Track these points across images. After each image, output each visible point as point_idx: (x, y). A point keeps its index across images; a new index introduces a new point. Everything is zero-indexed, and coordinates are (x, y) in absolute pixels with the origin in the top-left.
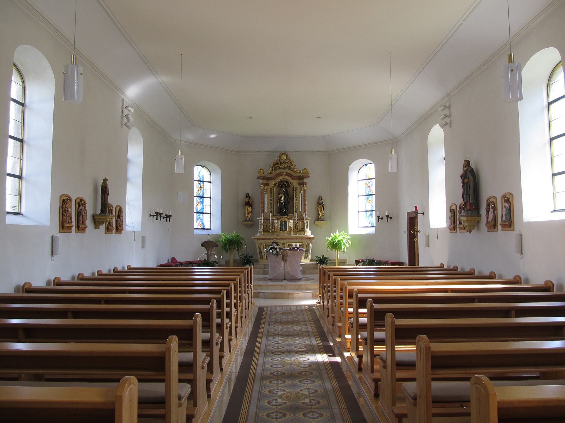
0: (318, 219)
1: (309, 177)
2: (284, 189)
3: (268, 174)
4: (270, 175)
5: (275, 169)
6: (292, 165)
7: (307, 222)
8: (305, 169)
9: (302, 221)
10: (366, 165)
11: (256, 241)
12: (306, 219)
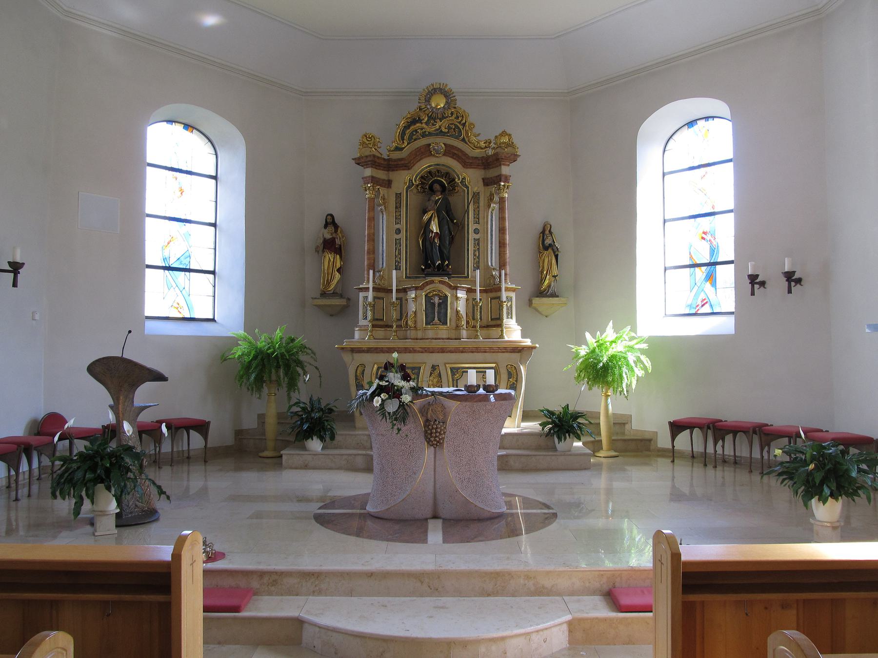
0: (541, 293)
1: (514, 158)
2: (438, 197)
3: (390, 151)
4: (396, 155)
5: (410, 138)
6: (464, 125)
7: (509, 299)
8: (504, 133)
9: (493, 295)
10: (691, 124)
11: (347, 357)
12: (507, 289)
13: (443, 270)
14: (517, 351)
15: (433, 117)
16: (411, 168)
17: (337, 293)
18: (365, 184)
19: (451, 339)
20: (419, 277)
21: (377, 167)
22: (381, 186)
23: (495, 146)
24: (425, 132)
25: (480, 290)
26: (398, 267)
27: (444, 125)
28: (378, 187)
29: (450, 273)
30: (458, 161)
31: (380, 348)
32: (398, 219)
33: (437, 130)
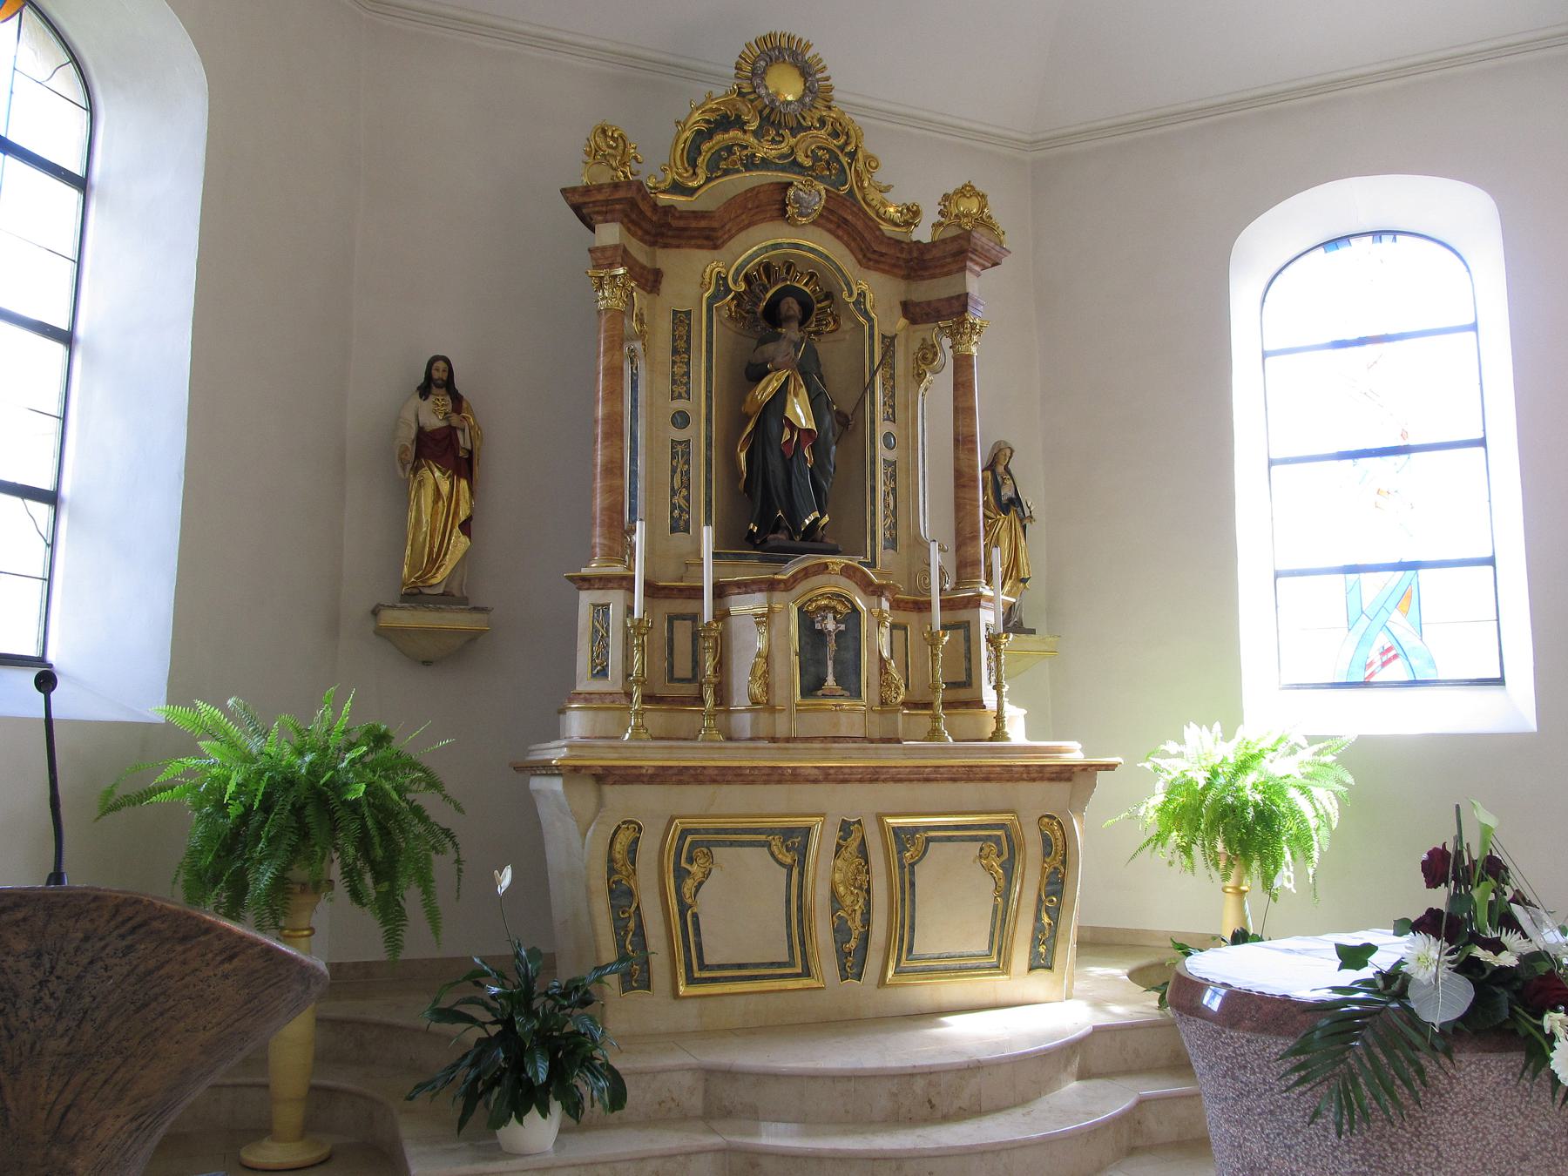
5: (713, 166)
6: (852, 156)
15: (773, 119)
16: (724, 243)
19: (872, 741)
20: (745, 557)
25: (940, 600)
26: (682, 523)
27: (804, 146)
30: (848, 246)
32: (680, 385)
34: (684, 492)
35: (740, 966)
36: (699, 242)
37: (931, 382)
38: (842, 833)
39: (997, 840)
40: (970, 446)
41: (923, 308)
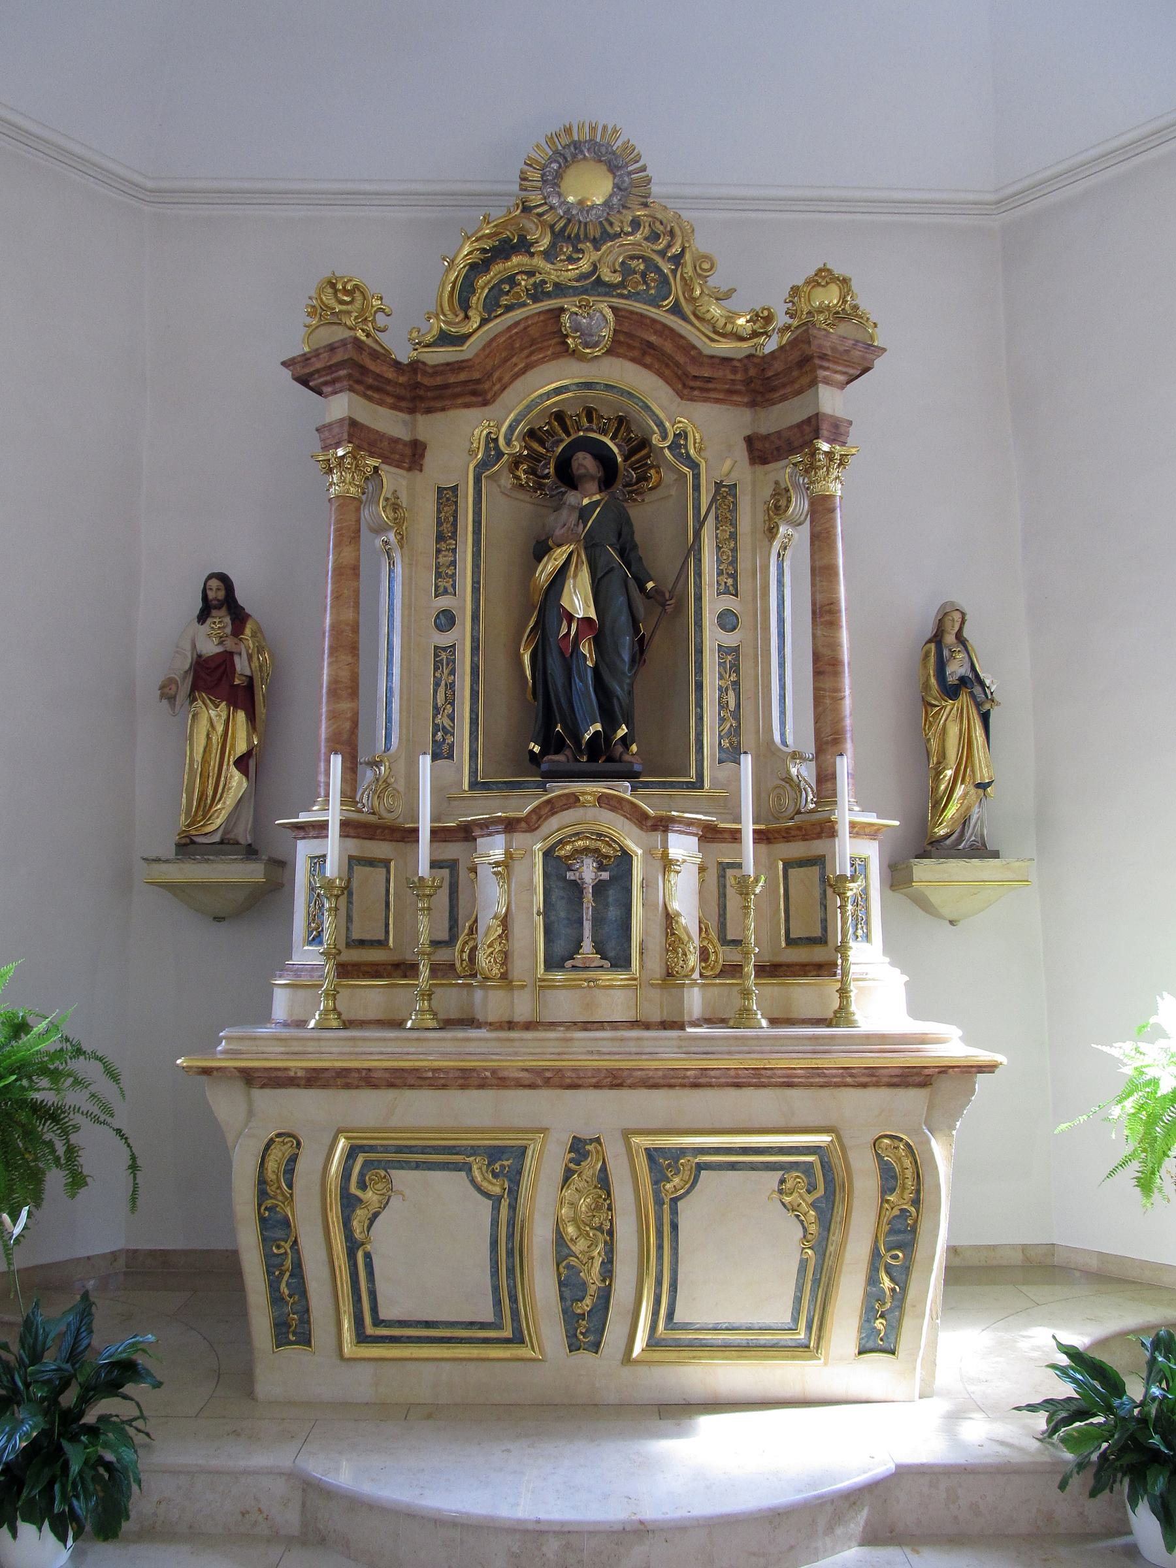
5: (492, 307)
6: (677, 259)
9: (797, 849)
12: (858, 830)
13: (610, 759)
14: (917, 1079)
17: (238, 843)
18: (326, 448)
19: (647, 1026)
21: (369, 393)
22: (386, 460)
23: (790, 321)
24: (544, 282)
25: (755, 831)
26: (445, 747)
27: (610, 258)
28: (372, 462)
29: (637, 768)
30: (661, 375)
31: (358, 1070)
33: (582, 277)
34: (449, 709)
35: (428, 1324)
36: (468, 399)
37: (789, 537)
38: (572, 1155)
39: (807, 1169)
40: (827, 618)
41: (773, 442)
